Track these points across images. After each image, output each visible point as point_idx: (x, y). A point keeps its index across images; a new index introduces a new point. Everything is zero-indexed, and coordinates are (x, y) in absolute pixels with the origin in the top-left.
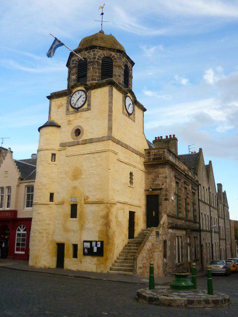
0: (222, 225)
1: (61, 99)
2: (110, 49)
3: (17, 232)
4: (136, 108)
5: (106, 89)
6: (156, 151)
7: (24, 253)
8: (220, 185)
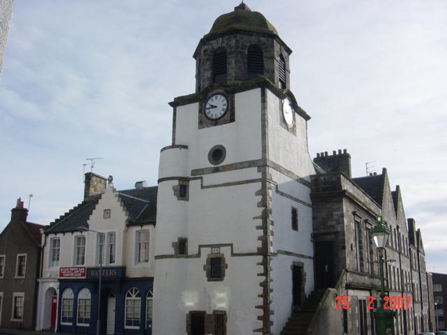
0: (416, 281)
1: (365, 292)
2: (258, 34)
3: (127, 298)
4: (297, 116)
5: (258, 90)
6: (326, 177)
7: (138, 328)
8: (411, 222)
